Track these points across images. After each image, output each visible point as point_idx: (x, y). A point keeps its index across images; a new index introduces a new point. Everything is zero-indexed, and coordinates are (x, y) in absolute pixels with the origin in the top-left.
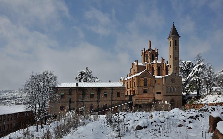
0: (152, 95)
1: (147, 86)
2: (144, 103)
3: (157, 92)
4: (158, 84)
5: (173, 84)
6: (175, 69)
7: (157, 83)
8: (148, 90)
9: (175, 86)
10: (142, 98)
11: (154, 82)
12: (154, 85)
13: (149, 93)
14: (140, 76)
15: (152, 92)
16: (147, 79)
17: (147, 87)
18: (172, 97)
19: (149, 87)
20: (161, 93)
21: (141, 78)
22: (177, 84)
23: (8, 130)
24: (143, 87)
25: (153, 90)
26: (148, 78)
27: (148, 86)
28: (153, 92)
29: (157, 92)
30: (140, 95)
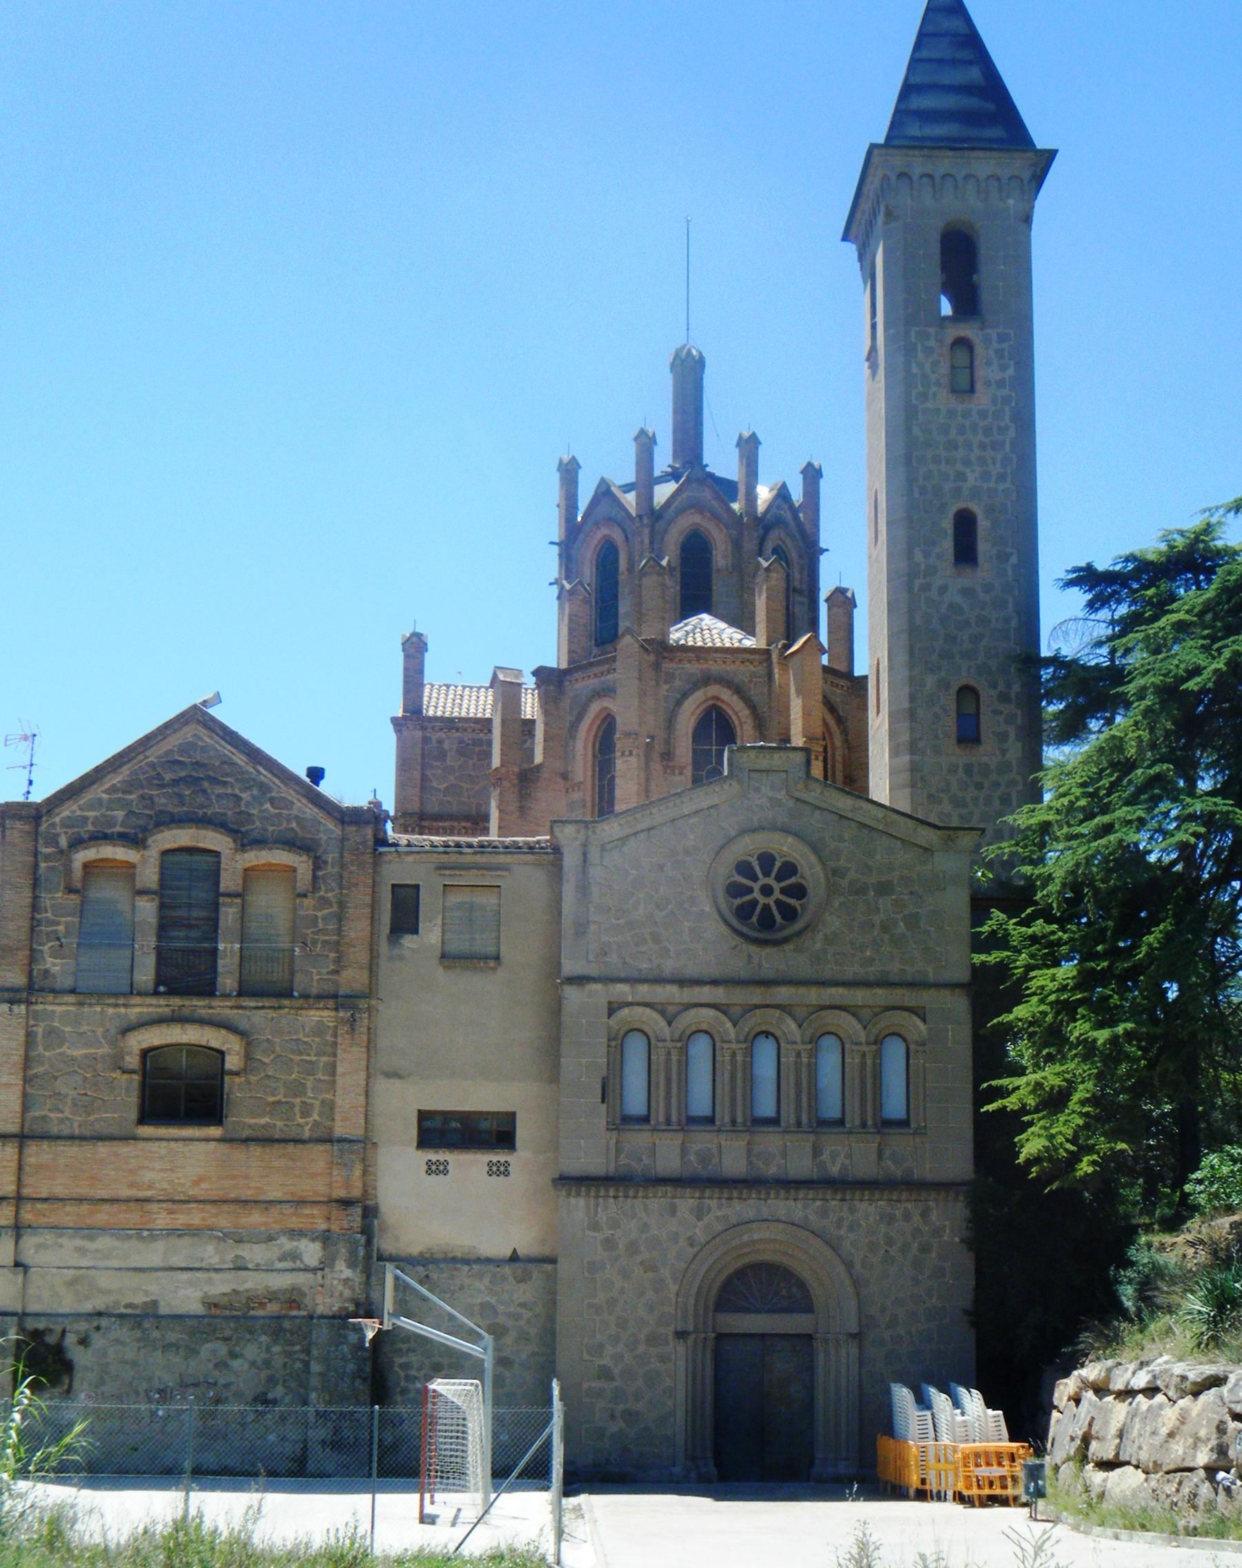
0: (318, 1157)
1: (209, 990)
2: (136, 1292)
3: (423, 1116)
4: (448, 958)
5: (769, 960)
6: (950, 723)
7: (431, 934)
8: (232, 1062)
9: (814, 996)
10: (103, 1216)
11: (357, 929)
12: (353, 978)
13: (242, 1117)
14: (68, 810)
15: (329, 1108)
16: (215, 874)
17: (221, 1008)
18: (744, 1207)
19: (258, 1017)
20: (522, 1134)
21: (101, 837)
22: (853, 970)
23: (185, 1517)
24: (139, 1009)
25: (350, 1060)
26: (245, 841)
27: (227, 982)
28: (348, 1098)
29: (423, 1116)
30: (70, 1151)
